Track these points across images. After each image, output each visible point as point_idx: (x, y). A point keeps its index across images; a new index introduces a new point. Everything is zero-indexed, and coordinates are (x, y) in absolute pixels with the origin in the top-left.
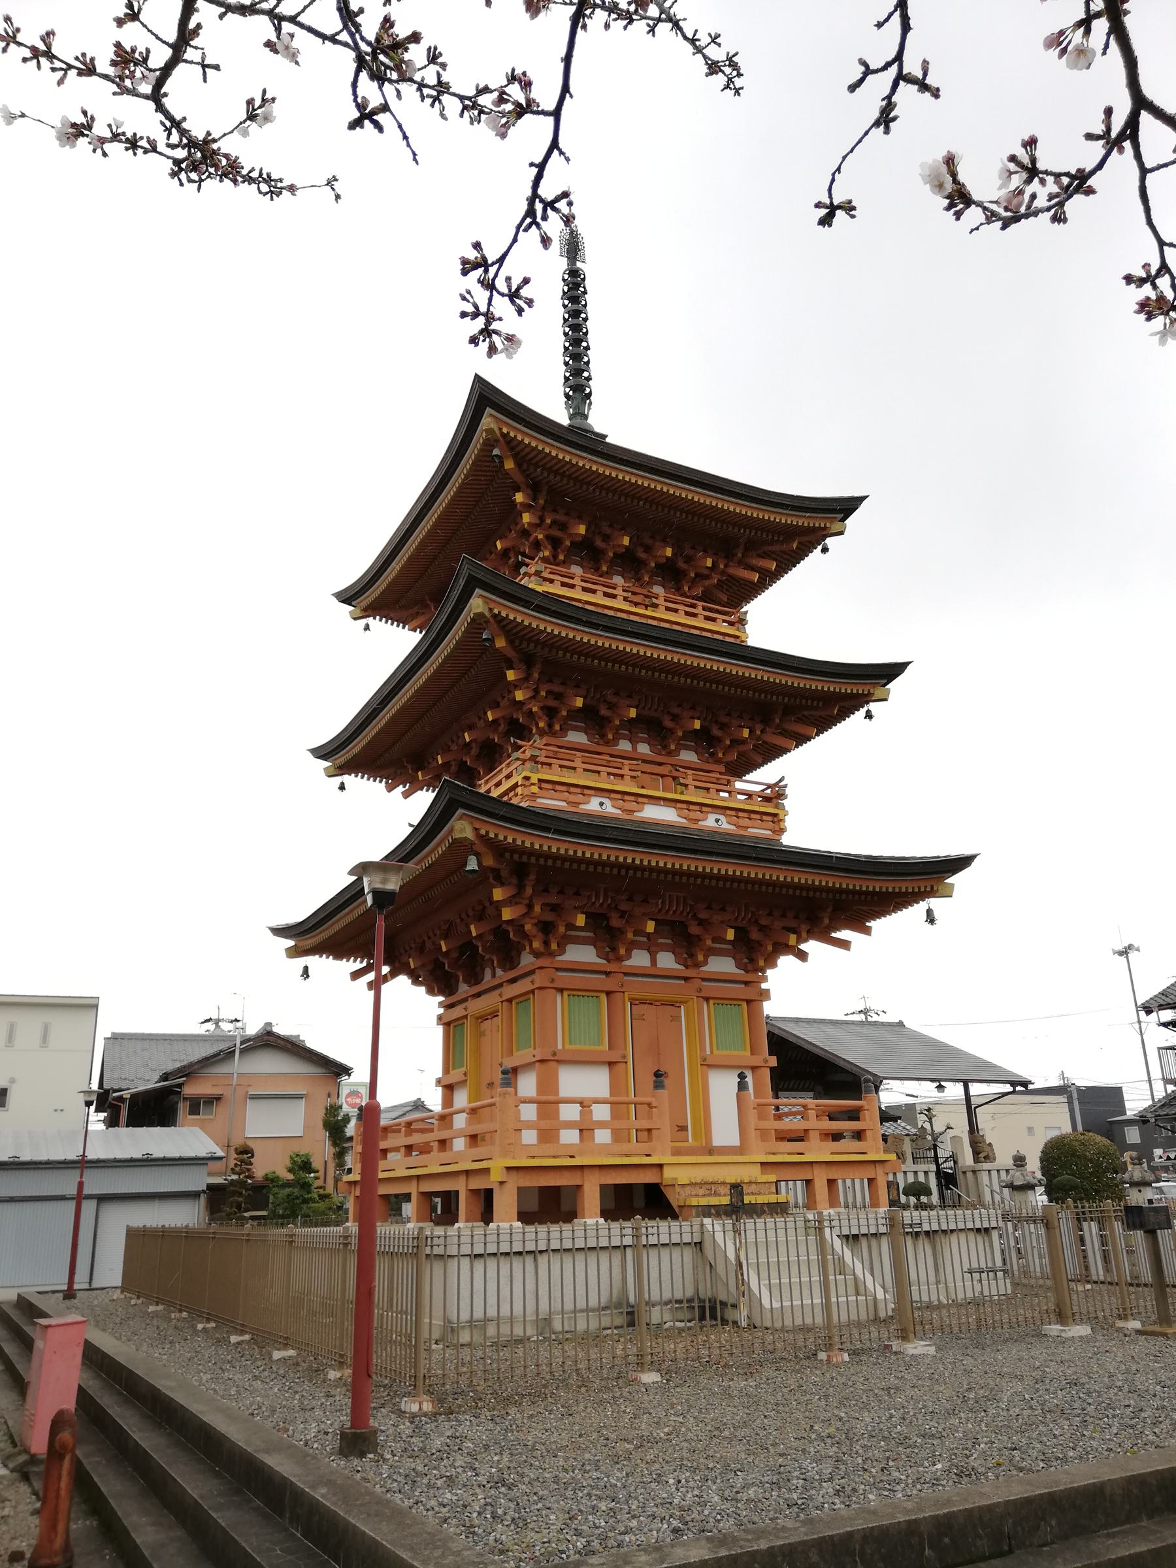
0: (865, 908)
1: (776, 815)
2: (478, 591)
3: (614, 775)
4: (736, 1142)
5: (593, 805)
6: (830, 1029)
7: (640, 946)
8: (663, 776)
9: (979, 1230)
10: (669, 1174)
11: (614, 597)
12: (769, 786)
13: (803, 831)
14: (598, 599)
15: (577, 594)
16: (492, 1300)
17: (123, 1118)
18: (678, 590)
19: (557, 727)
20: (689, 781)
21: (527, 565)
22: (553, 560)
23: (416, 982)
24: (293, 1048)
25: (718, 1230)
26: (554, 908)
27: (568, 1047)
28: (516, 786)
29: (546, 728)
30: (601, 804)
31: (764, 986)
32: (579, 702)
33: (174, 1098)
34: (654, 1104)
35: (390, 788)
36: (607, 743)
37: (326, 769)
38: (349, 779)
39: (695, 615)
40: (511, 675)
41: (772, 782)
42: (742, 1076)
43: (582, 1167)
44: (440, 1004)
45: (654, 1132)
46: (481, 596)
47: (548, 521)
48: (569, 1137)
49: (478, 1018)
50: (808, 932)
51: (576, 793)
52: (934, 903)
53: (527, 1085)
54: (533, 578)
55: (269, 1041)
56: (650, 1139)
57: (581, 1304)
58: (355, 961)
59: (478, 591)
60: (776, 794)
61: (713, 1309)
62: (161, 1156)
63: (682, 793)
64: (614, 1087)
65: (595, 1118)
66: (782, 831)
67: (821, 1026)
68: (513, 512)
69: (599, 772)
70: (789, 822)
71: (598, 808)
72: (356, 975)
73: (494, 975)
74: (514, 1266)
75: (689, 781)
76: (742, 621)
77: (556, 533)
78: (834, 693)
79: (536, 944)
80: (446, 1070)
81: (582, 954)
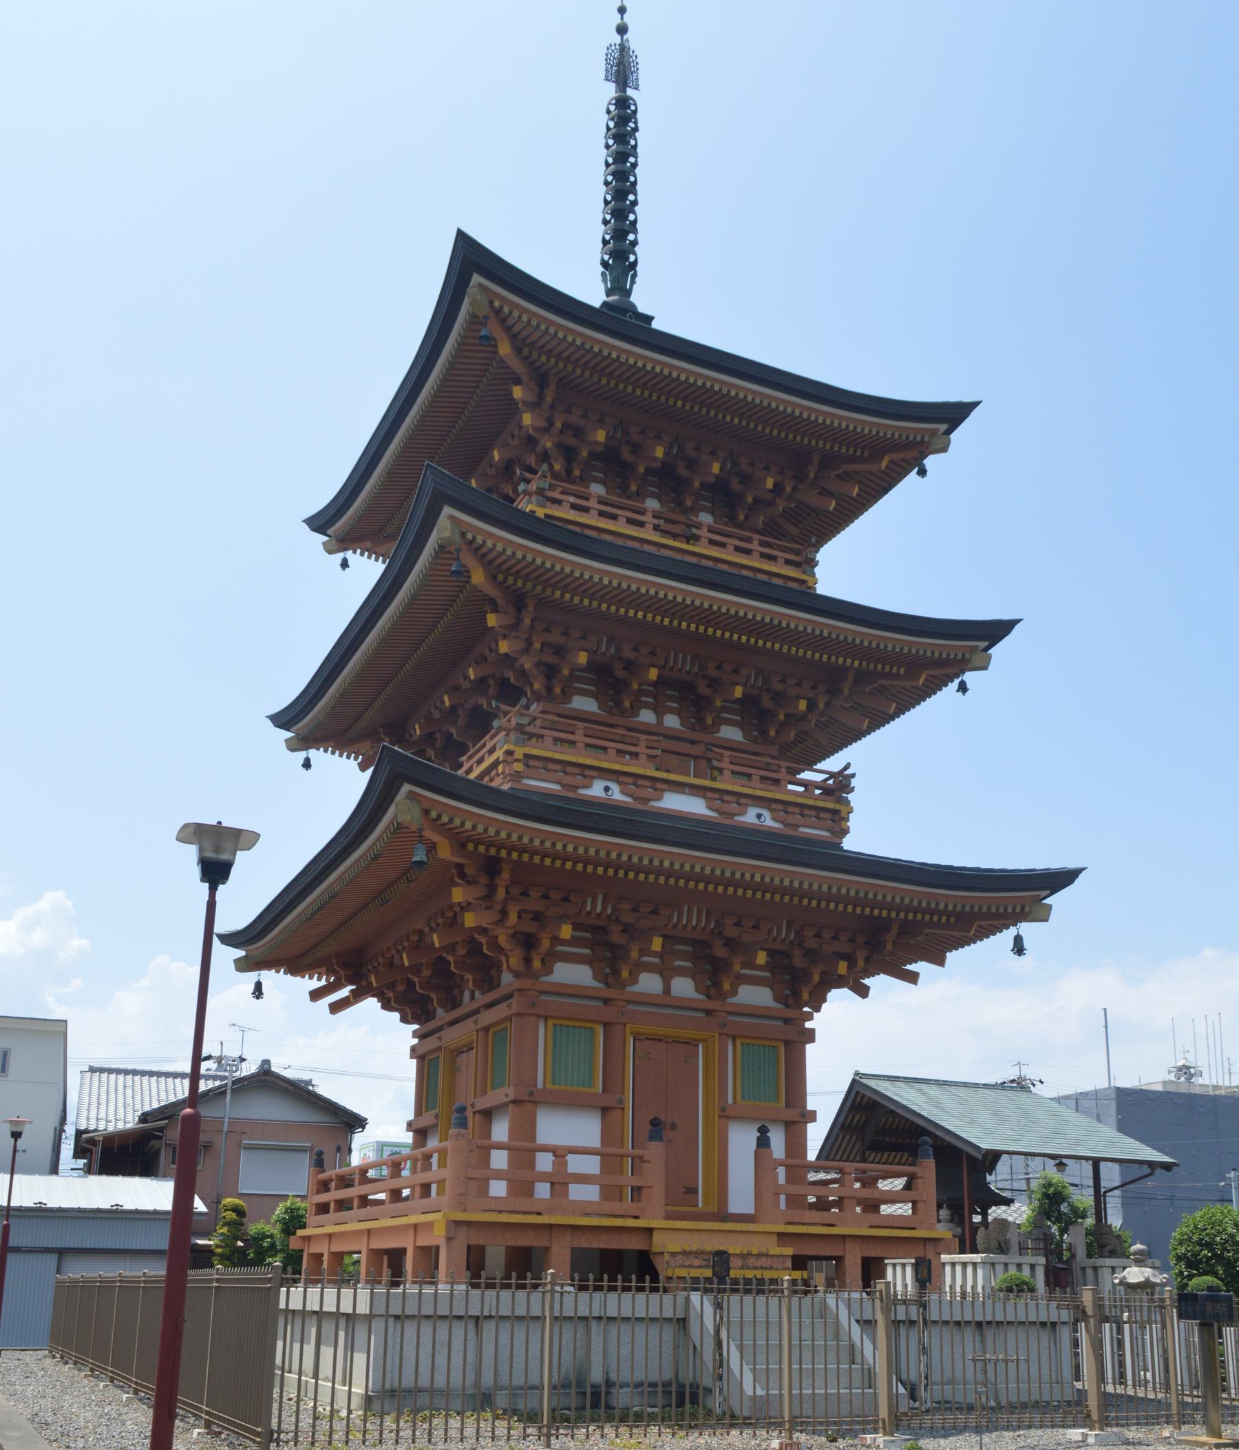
0: (957, 934)
1: (836, 812)
3: (563, 741)
4: (750, 1210)
5: (597, 790)
6: (933, 1091)
7: (649, 968)
8: (695, 758)
9: (1043, 1324)
10: (657, 1238)
11: (641, 524)
14: (621, 527)
15: (591, 520)
17: (96, 1166)
19: (558, 690)
20: (725, 764)
24: (300, 1092)
25: (701, 1305)
26: (537, 917)
27: (549, 1086)
28: (496, 764)
29: (544, 692)
30: (607, 789)
31: (808, 1025)
34: (646, 1158)
36: (623, 713)
37: (287, 741)
38: (316, 755)
39: (748, 552)
42: (763, 1131)
43: (551, 1227)
45: (645, 1191)
47: (558, 425)
48: (543, 1190)
49: (453, 1051)
52: (1027, 929)
53: (501, 1131)
54: (534, 498)
55: (267, 1080)
58: (311, 978)
60: (841, 784)
62: (132, 1207)
63: (713, 779)
65: (571, 1170)
66: (845, 831)
67: (924, 1087)
68: (513, 409)
69: (605, 749)
70: (853, 822)
72: (316, 995)
73: (472, 997)
76: (813, 563)
77: (569, 440)
78: (938, 653)
79: (513, 961)
80: (419, 1111)
81: (573, 974)
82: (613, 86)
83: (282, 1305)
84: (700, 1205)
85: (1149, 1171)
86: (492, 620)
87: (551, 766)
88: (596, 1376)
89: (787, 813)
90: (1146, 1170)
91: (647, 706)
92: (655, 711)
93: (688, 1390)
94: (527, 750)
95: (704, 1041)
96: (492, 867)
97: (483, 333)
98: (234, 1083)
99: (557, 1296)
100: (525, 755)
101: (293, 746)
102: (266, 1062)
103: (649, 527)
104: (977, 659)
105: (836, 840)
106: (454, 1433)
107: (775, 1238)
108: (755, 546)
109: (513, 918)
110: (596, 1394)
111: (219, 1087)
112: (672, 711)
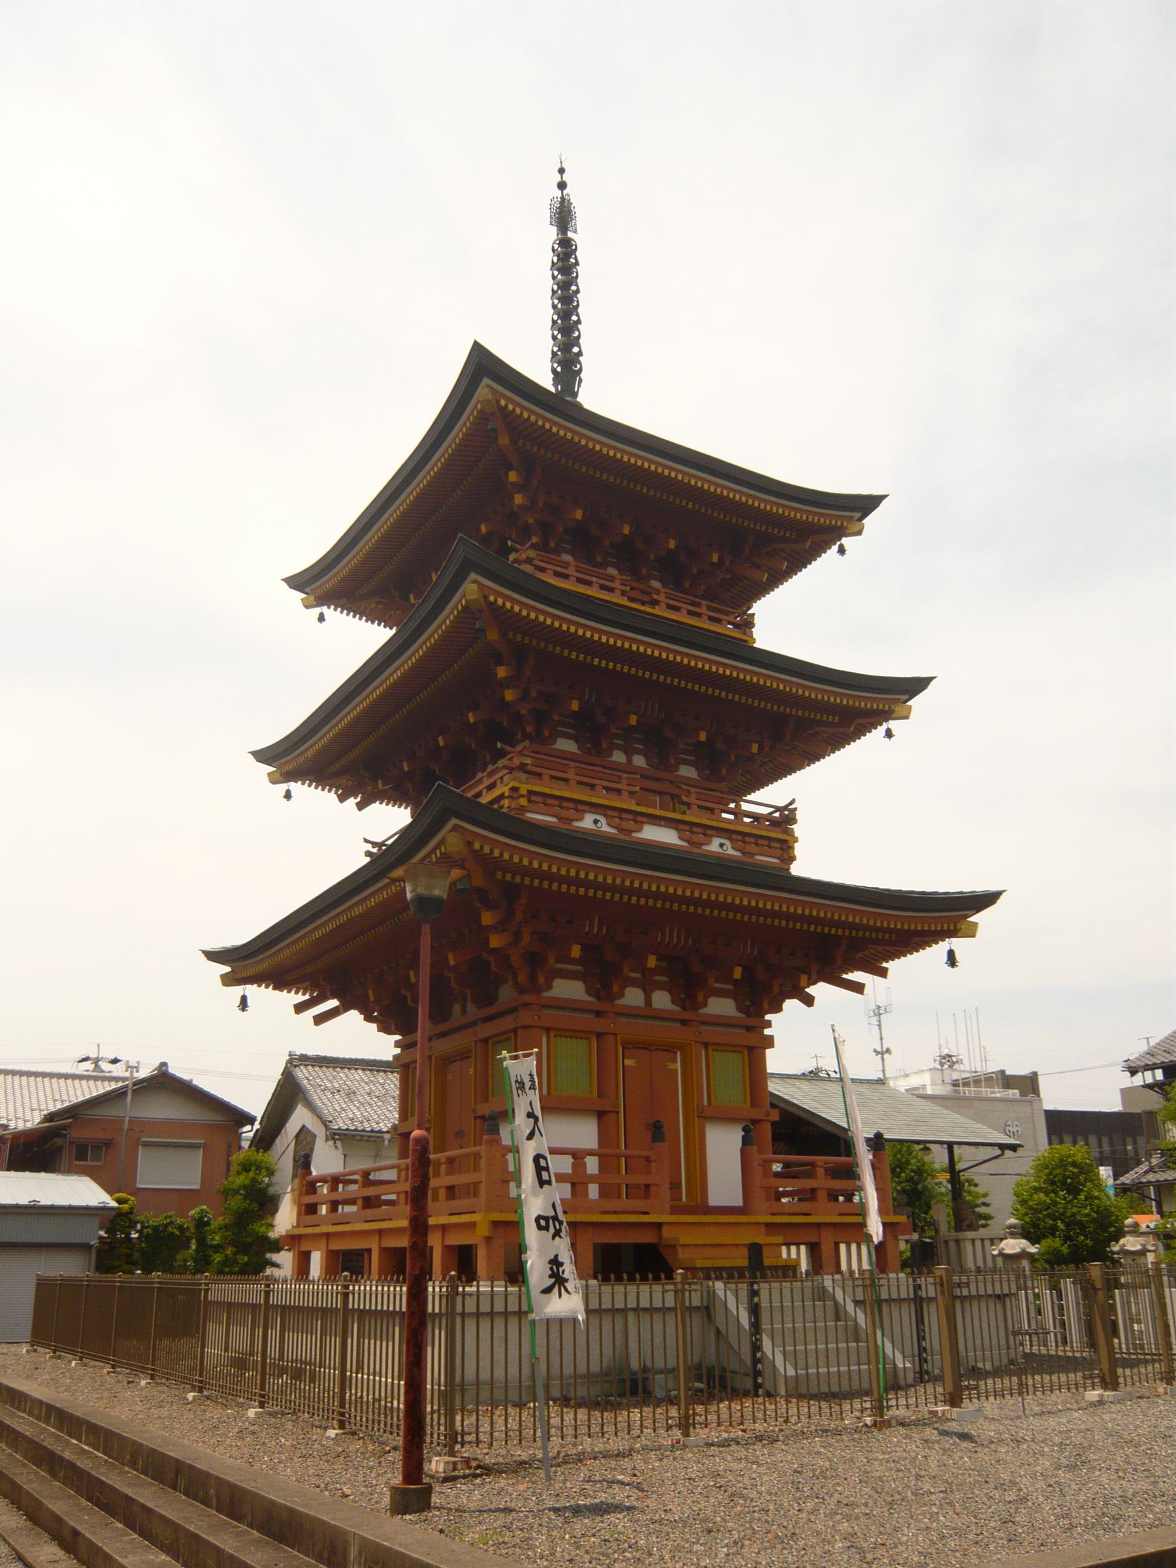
1: (785, 842)
2: (473, 576)
4: (738, 1201)
5: (587, 822)
7: (634, 983)
10: (667, 1233)
12: (778, 809)
13: (812, 861)
16: (485, 1363)
18: (678, 587)
21: (517, 551)
22: (542, 547)
23: (369, 1018)
25: (730, 1298)
28: (502, 797)
30: (596, 822)
31: (767, 1032)
32: (575, 706)
33: (58, 1141)
34: (653, 1158)
35: (342, 799)
37: (269, 774)
38: (296, 787)
40: (502, 672)
41: (782, 804)
44: (397, 1044)
45: (653, 1189)
46: (475, 582)
50: (818, 973)
51: (569, 808)
52: (956, 944)
55: (163, 1082)
56: (647, 1195)
57: (582, 1369)
58: (297, 993)
59: (473, 576)
60: (785, 818)
61: (723, 1379)
63: (684, 813)
64: (604, 1136)
66: (792, 859)
70: (798, 849)
71: (593, 827)
72: (300, 1008)
73: (464, 1012)
74: (604, 1322)
75: (692, 799)
76: (749, 624)
78: (848, 706)
81: (569, 989)
82: (554, 229)
83: (430, 1310)
84: (684, 1199)
85: (999, 1152)
86: (502, 672)
87: (549, 801)
88: (635, 1365)
89: (744, 842)
90: (998, 1152)
91: (619, 748)
92: (626, 752)
93: (717, 1373)
94: (529, 787)
95: (681, 1047)
96: (511, 892)
97: (490, 426)
98: (135, 1084)
99: (687, 1294)
100: (529, 792)
101: (274, 779)
102: (164, 1064)
103: (618, 592)
104: (898, 709)
105: (785, 867)
106: (595, 1429)
107: (763, 1229)
108: (703, 610)
109: (526, 938)
110: (634, 1382)
111: (122, 1088)
112: (639, 752)
